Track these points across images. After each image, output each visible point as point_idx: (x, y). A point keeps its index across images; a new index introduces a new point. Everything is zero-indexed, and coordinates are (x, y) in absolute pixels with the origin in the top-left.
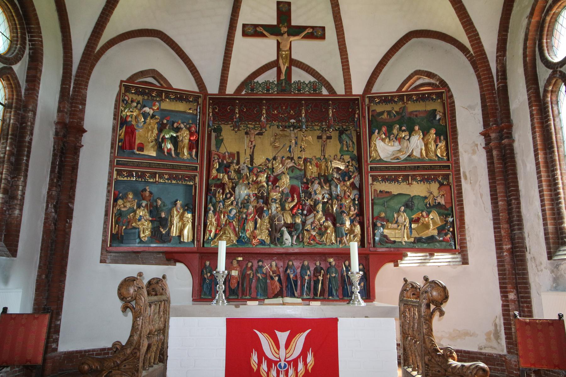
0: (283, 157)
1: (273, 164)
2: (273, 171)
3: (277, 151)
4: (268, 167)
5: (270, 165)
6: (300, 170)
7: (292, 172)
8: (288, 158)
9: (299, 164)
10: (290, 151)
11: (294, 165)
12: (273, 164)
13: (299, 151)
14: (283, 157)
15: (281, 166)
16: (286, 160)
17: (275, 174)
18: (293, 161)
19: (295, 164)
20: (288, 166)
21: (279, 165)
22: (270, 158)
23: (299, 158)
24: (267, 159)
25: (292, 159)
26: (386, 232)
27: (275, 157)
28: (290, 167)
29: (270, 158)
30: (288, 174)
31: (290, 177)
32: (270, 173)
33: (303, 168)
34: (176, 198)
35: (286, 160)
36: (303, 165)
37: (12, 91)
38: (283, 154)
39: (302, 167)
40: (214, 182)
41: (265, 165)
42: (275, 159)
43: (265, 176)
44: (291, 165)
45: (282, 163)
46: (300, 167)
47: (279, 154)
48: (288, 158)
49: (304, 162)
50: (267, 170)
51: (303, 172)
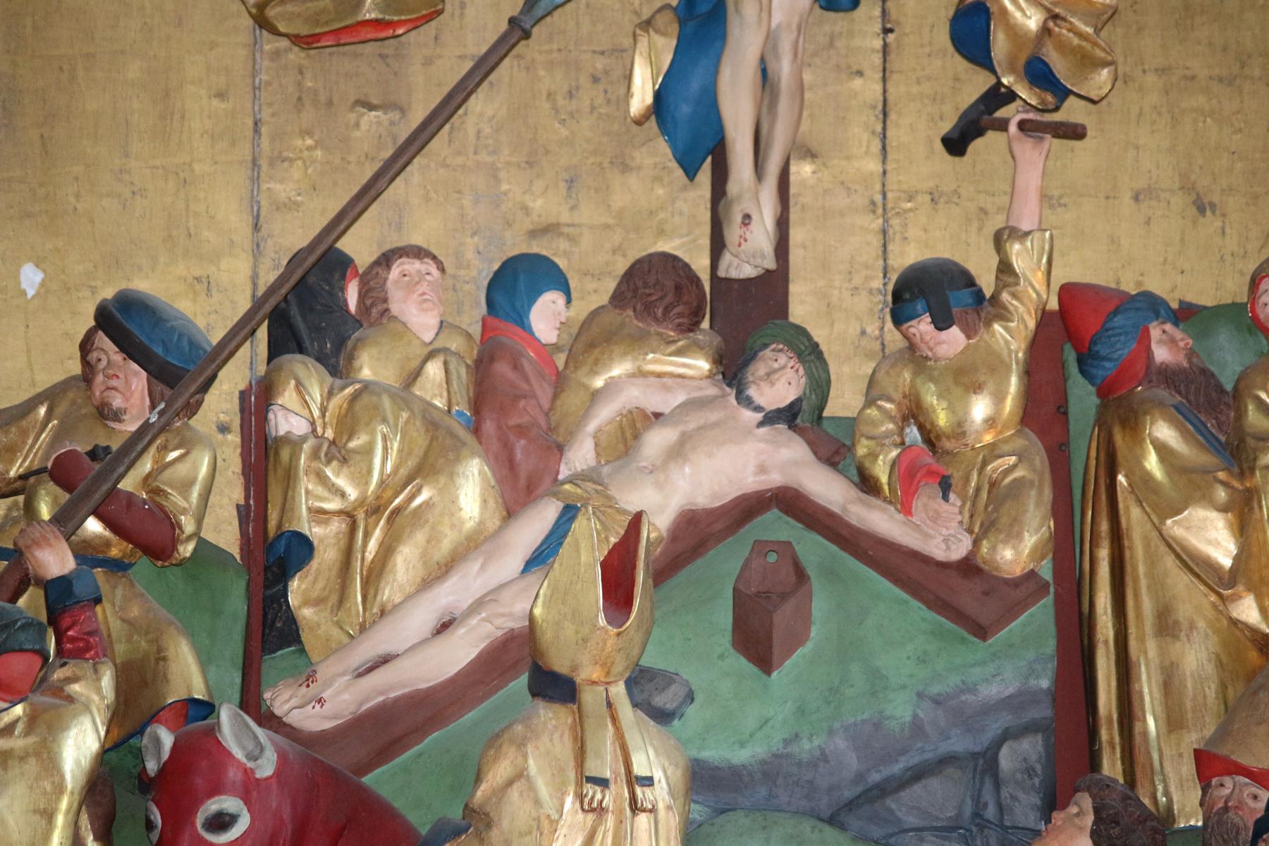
0: (517, 280)
1: (263, 459)
2: (272, 632)
3: (374, 133)
4: (148, 534)
5: (201, 483)
6: (960, 595)
7: (757, 642)
8: (657, 294)
9: (933, 460)
10: (699, 145)
11: (788, 461)
12: (263, 459)
13: (920, 129)
14: (517, 280)
15: (470, 491)
16: (591, 341)
17: (322, 700)
18: (778, 382)
19: (834, 449)
20: (661, 497)
21: (430, 464)
22: (212, 291)
23: (930, 292)
24: (126, 324)
25: (741, 318)
26: (272, 185)
27: (319, 270)
28: (698, 533)
29: (212, 291)
30: (653, 694)
31: (707, 783)
32: (187, 674)
33: (1019, 551)
34: (574, 302)
35: (591, 341)
36: (1021, 465)
37: (1143, 508)
38: (531, 206)
39: (990, 517)
40: (735, 264)
41: (83, 477)
42: (311, 311)
43: (80, 744)
44: (741, 459)
45: (508, 408)
46: (939, 532)
47: (418, 209)
48: (657, 294)
49: (1043, 412)
50: (117, 611)
51: (1017, 662)
